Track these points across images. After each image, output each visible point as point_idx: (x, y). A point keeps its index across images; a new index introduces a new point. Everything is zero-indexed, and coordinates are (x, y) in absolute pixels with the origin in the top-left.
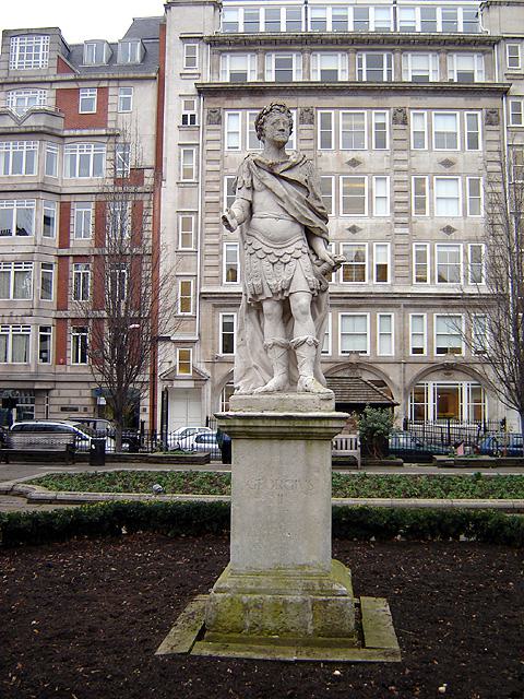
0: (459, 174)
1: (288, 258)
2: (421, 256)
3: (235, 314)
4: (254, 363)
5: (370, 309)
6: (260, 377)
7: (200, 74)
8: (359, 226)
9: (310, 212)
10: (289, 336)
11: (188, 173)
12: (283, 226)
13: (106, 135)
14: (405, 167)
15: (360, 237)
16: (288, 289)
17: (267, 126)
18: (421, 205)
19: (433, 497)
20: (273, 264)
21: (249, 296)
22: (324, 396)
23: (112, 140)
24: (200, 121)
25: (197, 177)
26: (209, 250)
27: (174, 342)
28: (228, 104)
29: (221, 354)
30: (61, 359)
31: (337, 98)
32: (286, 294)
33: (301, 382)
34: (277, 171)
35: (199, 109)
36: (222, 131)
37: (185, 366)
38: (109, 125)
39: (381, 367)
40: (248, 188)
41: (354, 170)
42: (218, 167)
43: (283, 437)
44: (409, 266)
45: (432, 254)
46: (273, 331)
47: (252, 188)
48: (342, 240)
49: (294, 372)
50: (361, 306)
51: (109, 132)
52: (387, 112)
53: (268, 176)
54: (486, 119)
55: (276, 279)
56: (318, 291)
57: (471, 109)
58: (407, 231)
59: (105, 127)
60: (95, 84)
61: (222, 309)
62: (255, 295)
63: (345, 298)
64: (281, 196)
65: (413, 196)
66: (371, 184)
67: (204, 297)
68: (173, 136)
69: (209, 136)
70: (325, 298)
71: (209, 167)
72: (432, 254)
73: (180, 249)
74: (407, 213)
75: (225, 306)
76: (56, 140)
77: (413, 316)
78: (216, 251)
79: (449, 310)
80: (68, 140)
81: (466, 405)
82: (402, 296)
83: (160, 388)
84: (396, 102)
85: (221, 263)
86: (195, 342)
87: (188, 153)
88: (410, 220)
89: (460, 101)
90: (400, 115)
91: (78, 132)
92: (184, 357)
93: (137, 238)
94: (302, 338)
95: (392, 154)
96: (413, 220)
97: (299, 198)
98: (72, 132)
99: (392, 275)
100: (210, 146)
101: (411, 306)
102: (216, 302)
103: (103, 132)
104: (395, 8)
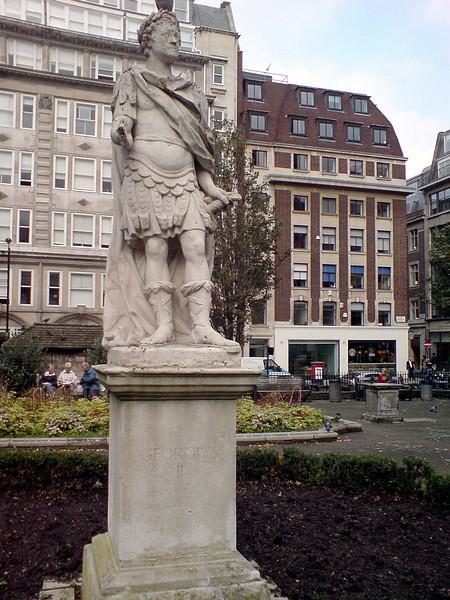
1: (178, 190)
4: (132, 309)
5: (95, 270)
6: (139, 326)
8: (90, 200)
12: (175, 152)
15: (89, 209)
16: (179, 227)
20: (163, 195)
31: (72, 90)
32: (177, 231)
34: (172, 87)
39: (16, 314)
40: (133, 105)
41: (84, 153)
43: (186, 396)
46: (156, 271)
47: (136, 106)
48: (73, 211)
50: (87, 267)
55: (167, 213)
62: (139, 230)
64: (176, 117)
74: (49, 185)
77: (72, 274)
94: (200, 283)
97: (192, 123)
104: (125, 20)
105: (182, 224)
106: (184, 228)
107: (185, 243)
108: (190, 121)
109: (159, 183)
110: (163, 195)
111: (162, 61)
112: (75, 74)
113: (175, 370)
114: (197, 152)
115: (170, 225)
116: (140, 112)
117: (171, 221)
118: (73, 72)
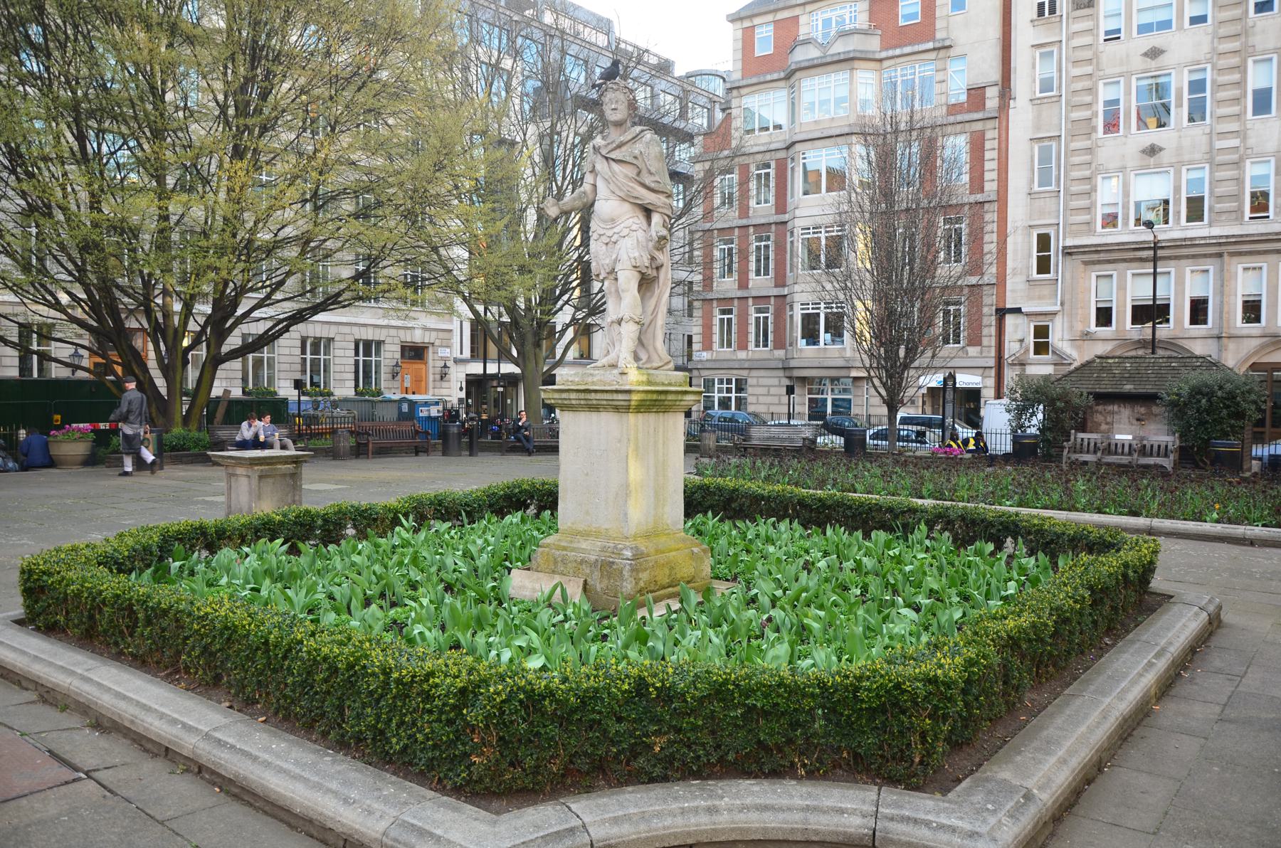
3: (1115, 274)
5: (1173, 262)
13: (934, 49)
23: (942, 53)
27: (1027, 315)
30: (743, 346)
37: (1041, 348)
38: (939, 35)
39: (1181, 342)
42: (1089, 69)
51: (938, 45)
59: (933, 39)
60: (770, 18)
61: (1098, 267)
63: (1235, 243)
67: (1068, 252)
68: (1025, 33)
69: (1077, 27)
73: (1036, 188)
75: (1099, 262)
76: (872, 64)
80: (886, 64)
86: (1055, 314)
91: (898, 52)
92: (1042, 332)
93: (977, 183)
98: (891, 53)
100: (1077, 42)
103: (930, 45)
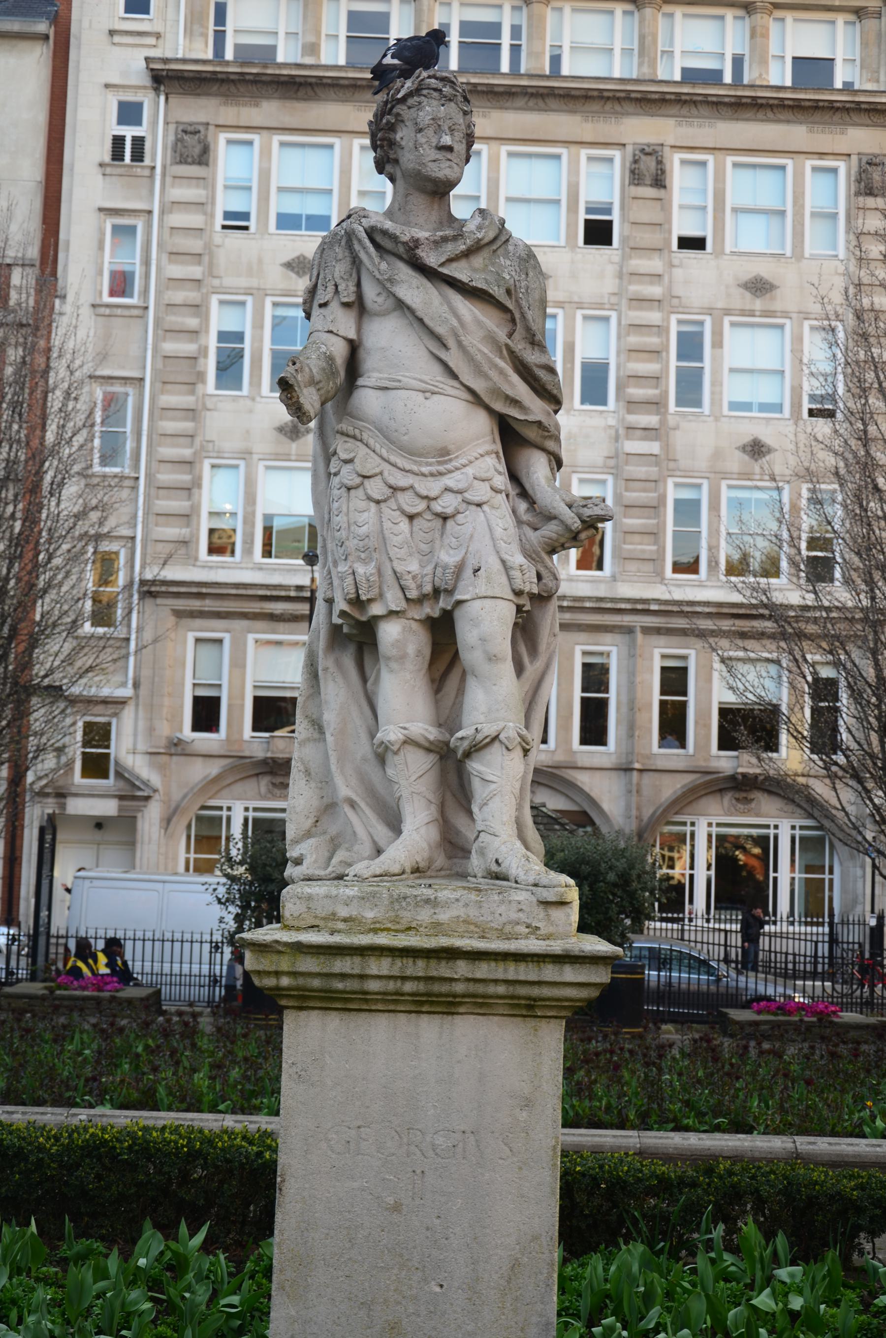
0: (786, 314)
1: (448, 503)
2: (687, 510)
7: (158, 36)
9: (515, 378)
10: (449, 720)
11: (121, 284)
14: (655, 291)
16: (450, 592)
17: (403, 135)
18: (690, 388)
19: (749, 1130)
20: (411, 518)
21: (341, 605)
22: (550, 895)
24: (158, 152)
25: (145, 292)
26: (166, 477)
28: (229, 113)
29: (187, 732)
33: (482, 853)
34: (432, 259)
35: (154, 123)
36: (207, 182)
42: (196, 271)
44: (655, 535)
45: (715, 506)
47: (358, 307)
49: (459, 821)
52: (617, 154)
53: (404, 271)
54: (859, 181)
56: (533, 597)
57: (822, 155)
58: (654, 447)
61: (198, 622)
62: (358, 602)
64: (440, 330)
65: (673, 363)
66: (570, 329)
67: (151, 591)
68: (88, 187)
70: (550, 618)
71: (176, 270)
72: (715, 506)
74: (657, 405)
78: (185, 478)
79: (750, 644)
81: (786, 877)
82: (640, 608)
83: (34, 816)
84: (642, 129)
85: (662, 526)
86: (122, 702)
87: (124, 232)
88: (663, 422)
89: (796, 134)
90: (649, 164)
95: (624, 258)
96: (671, 421)
97: (491, 339)
99: (614, 556)
100: (178, 219)
101: (658, 631)
102: (182, 604)
105: (455, 588)
106: (458, 597)
107: (468, 634)
108: (481, 333)
109: (403, 489)
110: (411, 518)
111: (423, 191)
112: (728, 78)
113: (533, 945)
114: (499, 406)
115: (428, 589)
116: (366, 319)
117: (428, 579)
118: (719, 73)
